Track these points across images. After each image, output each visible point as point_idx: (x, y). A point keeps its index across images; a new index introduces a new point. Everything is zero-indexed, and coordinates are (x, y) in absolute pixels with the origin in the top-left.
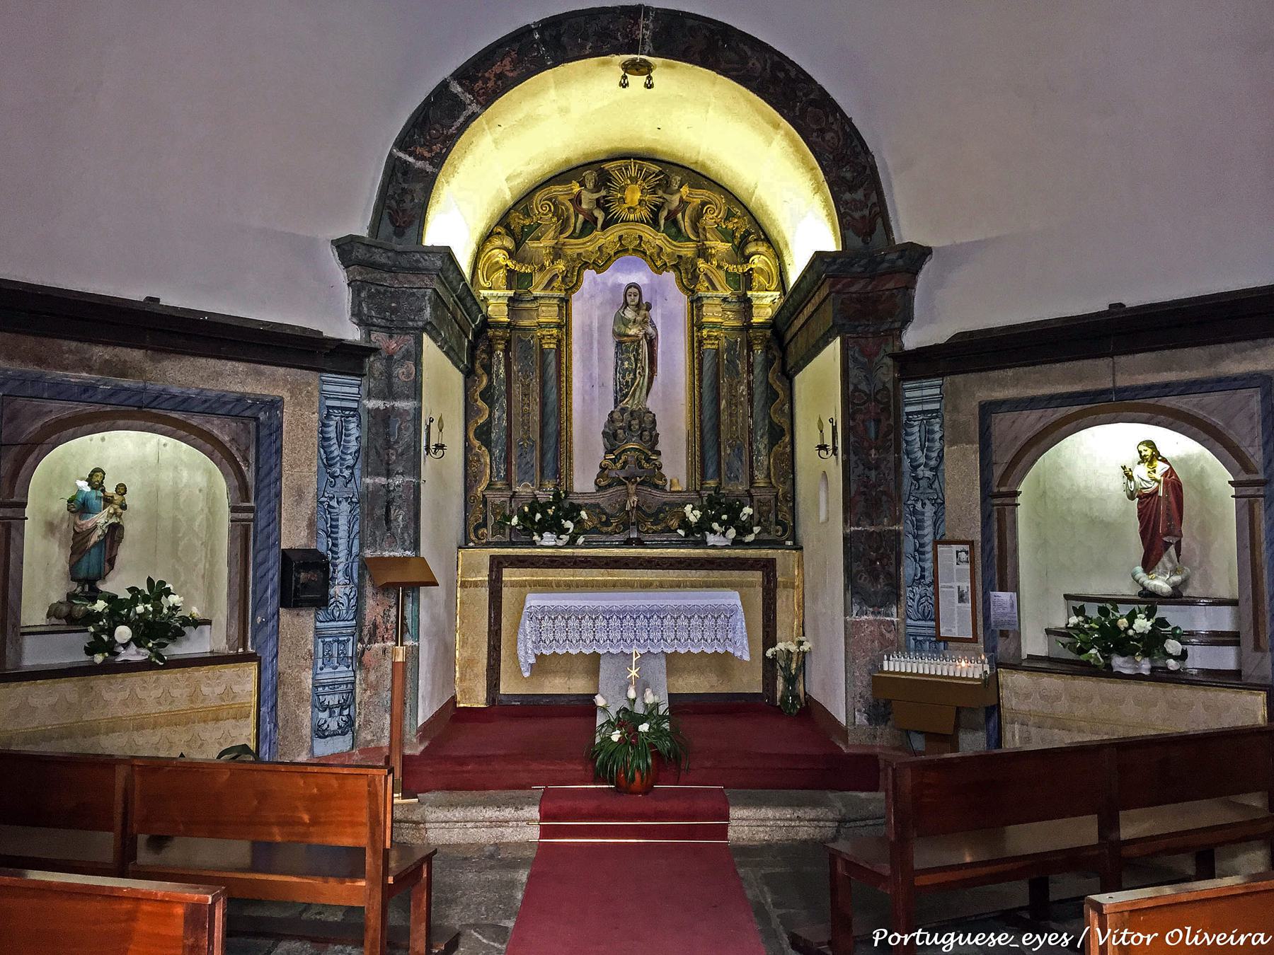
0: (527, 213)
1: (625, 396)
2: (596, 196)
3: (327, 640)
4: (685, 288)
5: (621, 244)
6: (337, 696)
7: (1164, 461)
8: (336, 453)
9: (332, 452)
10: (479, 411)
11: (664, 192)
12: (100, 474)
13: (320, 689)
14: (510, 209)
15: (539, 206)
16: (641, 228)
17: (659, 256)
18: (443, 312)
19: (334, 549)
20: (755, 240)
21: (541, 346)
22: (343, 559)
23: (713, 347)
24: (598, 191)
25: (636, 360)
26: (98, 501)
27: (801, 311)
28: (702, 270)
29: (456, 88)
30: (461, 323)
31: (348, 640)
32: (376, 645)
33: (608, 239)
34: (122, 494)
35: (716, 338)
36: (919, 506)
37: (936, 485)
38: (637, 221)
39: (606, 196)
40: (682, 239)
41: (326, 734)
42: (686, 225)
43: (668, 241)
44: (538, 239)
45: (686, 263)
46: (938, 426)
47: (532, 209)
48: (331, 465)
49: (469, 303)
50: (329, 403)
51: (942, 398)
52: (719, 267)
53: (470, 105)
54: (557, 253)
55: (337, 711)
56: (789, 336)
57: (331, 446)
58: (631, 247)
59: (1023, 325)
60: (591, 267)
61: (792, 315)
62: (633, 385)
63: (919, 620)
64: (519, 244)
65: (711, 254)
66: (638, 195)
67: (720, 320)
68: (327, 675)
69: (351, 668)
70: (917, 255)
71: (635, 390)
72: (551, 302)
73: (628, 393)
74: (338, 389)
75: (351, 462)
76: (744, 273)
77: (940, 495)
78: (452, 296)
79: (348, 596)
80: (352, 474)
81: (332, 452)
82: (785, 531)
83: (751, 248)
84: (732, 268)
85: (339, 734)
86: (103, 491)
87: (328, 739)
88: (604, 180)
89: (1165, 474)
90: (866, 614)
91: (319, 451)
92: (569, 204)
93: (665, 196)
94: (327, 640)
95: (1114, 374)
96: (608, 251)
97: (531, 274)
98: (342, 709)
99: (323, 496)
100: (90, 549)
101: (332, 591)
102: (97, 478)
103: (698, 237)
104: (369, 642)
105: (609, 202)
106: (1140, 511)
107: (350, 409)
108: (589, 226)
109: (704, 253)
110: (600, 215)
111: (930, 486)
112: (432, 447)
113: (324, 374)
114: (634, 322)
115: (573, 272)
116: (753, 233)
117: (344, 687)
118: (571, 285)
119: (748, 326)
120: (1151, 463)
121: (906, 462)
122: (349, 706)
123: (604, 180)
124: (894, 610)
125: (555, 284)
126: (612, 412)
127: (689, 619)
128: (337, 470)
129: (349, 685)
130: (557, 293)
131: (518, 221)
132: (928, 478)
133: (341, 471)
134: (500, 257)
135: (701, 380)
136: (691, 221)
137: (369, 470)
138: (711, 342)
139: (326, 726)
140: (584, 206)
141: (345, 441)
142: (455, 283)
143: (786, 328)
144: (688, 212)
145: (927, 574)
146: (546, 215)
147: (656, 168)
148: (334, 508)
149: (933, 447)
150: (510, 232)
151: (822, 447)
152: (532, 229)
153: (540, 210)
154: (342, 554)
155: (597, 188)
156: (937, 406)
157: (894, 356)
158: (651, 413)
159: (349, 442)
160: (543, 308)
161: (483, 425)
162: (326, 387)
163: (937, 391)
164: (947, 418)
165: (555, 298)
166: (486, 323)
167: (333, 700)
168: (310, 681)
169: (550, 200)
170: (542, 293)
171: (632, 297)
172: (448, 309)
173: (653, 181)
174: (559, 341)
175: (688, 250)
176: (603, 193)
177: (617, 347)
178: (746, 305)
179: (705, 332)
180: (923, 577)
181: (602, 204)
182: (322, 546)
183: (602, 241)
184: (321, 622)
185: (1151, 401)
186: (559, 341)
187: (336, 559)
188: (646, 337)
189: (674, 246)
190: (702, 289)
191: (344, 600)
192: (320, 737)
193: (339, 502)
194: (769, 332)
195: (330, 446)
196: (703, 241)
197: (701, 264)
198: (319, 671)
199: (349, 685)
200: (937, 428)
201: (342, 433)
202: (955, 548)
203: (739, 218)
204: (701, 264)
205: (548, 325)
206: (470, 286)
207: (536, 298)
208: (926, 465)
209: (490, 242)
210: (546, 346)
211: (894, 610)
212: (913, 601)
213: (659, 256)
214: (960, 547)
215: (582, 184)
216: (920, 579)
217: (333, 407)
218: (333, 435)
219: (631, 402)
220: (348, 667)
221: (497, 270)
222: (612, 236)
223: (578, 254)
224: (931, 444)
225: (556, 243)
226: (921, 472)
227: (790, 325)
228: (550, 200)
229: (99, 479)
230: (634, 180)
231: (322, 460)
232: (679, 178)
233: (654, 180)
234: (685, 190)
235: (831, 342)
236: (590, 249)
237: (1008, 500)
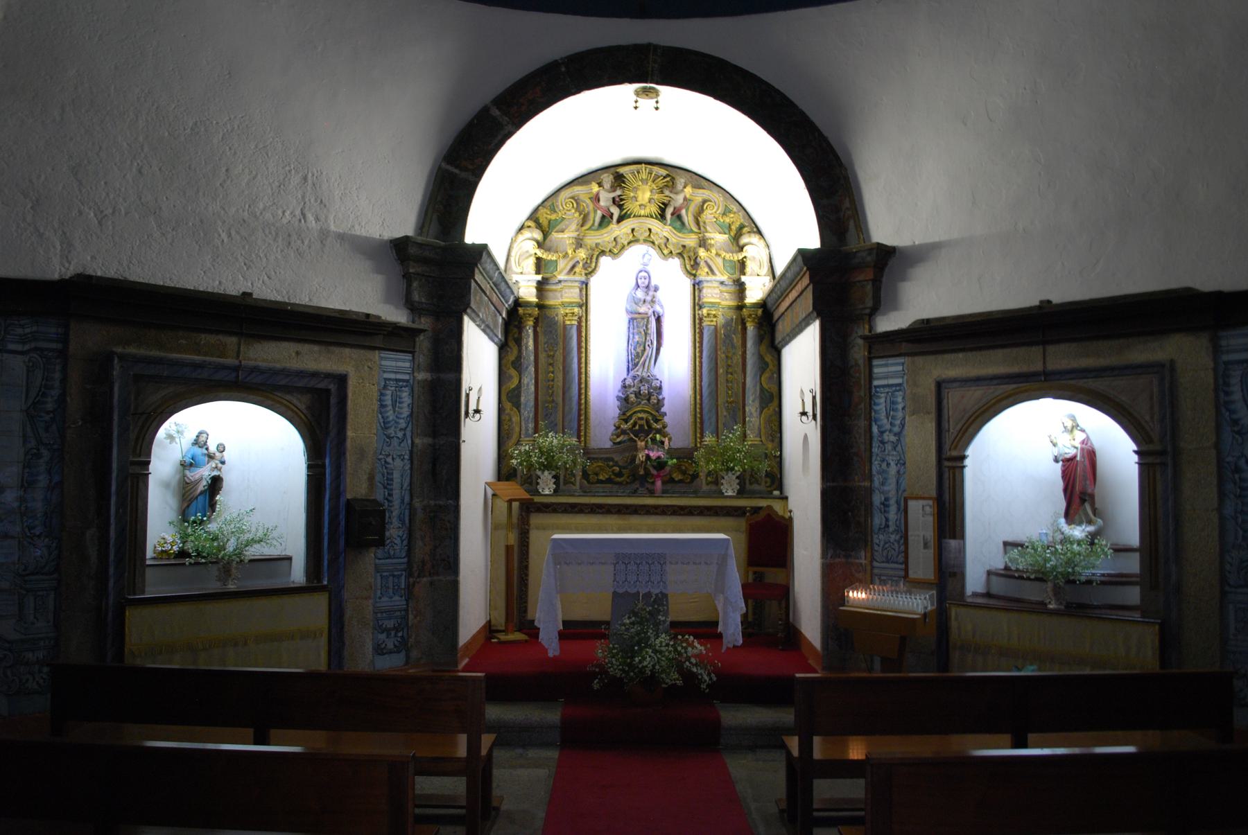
0: (553, 210)
1: (636, 365)
2: (613, 195)
3: (385, 574)
4: (689, 273)
5: (634, 235)
6: (392, 621)
7: (1083, 431)
8: (391, 418)
9: (388, 417)
10: (511, 377)
11: (671, 192)
12: (205, 435)
13: (379, 615)
14: (539, 206)
15: (564, 204)
16: (650, 222)
17: (666, 245)
18: (481, 297)
19: (390, 498)
20: (749, 232)
21: (564, 322)
22: (397, 507)
23: (712, 323)
24: (614, 191)
25: (646, 334)
26: (203, 457)
27: (788, 295)
28: (702, 258)
29: (496, 112)
30: (496, 305)
31: (402, 575)
32: (425, 579)
33: (621, 231)
34: (222, 452)
35: (715, 316)
36: (884, 465)
37: (899, 448)
38: (648, 216)
39: (621, 195)
40: (686, 231)
41: (385, 651)
42: (688, 218)
43: (674, 233)
44: (563, 231)
45: (689, 251)
46: (901, 398)
47: (558, 206)
48: (387, 428)
49: (503, 286)
50: (386, 376)
51: (904, 374)
52: (718, 255)
53: (506, 125)
54: (579, 243)
55: (393, 633)
56: (776, 317)
57: (387, 412)
58: (642, 238)
59: (971, 315)
60: (607, 254)
61: (780, 297)
62: (642, 355)
63: (883, 562)
64: (546, 235)
65: (710, 244)
66: (648, 195)
67: (718, 301)
68: (385, 602)
69: (403, 598)
70: (885, 254)
71: (645, 361)
72: (573, 285)
73: (638, 362)
74: (394, 364)
75: (403, 425)
76: (739, 261)
77: (902, 456)
78: (489, 283)
79: (401, 537)
80: (405, 435)
81: (388, 417)
82: (773, 482)
83: (744, 240)
84: (728, 256)
85: (394, 652)
86: (207, 449)
87: (386, 656)
88: (619, 180)
89: (1083, 442)
90: (839, 557)
91: (378, 417)
92: (588, 201)
93: (671, 195)
94: (385, 574)
95: (1044, 358)
96: (622, 241)
97: (556, 261)
98: (397, 631)
99: (381, 454)
100: (197, 497)
101: (387, 534)
102: (203, 438)
103: (700, 229)
104: (419, 577)
105: (622, 200)
106: (1063, 472)
107: (403, 381)
108: (606, 220)
109: (705, 243)
110: (616, 212)
111: (895, 448)
112: (471, 411)
113: (383, 352)
114: (644, 301)
115: (591, 259)
116: (747, 227)
117: (398, 613)
118: (590, 270)
119: (740, 307)
120: (1072, 431)
121: (875, 429)
122: (403, 629)
123: (619, 180)
124: (863, 553)
125: (577, 269)
126: (625, 379)
127: (638, 565)
128: (391, 431)
129: (403, 612)
130: (577, 278)
131: (544, 216)
132: (893, 442)
133: (396, 433)
134: (531, 247)
135: (701, 352)
136: (694, 216)
137: (419, 431)
138: (710, 319)
139: (384, 645)
140: (602, 203)
141: (399, 407)
142: (491, 272)
143: (774, 307)
144: (691, 209)
145: (890, 523)
146: (570, 210)
147: (663, 172)
148: (388, 463)
149: (896, 416)
150: (539, 226)
151: (804, 413)
152: (557, 222)
153: (565, 207)
154: (396, 503)
155: (613, 189)
156: (899, 381)
157: (865, 338)
158: (657, 379)
159: (401, 408)
160: (567, 290)
161: (514, 389)
162: (384, 363)
163: (900, 368)
164: (908, 392)
165: (576, 281)
166: (518, 303)
167: (390, 624)
168: (371, 608)
169: (573, 198)
170: (565, 278)
171: (643, 280)
172: (485, 294)
173: (660, 182)
174: (580, 318)
175: (691, 241)
176: (618, 192)
177: (629, 322)
178: (741, 288)
179: (705, 311)
180: (887, 526)
181: (619, 202)
182: (379, 495)
183: (617, 233)
184: (380, 559)
185: (1072, 382)
186: (580, 318)
187: (391, 506)
188: (654, 315)
189: (679, 237)
190: (703, 273)
191: (398, 541)
192: (379, 654)
193: (393, 459)
194: (760, 312)
195: (387, 412)
196: (704, 232)
197: (702, 253)
198: (378, 600)
199: (403, 612)
200: (900, 399)
201: (396, 401)
202: (921, 502)
203: (735, 213)
204: (702, 253)
205: (571, 304)
206: (503, 273)
207: (560, 282)
208: (890, 431)
209: (521, 233)
210: (568, 323)
211: (863, 553)
212: (879, 546)
213: (666, 245)
214: (925, 502)
215: (600, 185)
216: (884, 528)
217: (390, 379)
218: (389, 402)
219: (641, 370)
220: (401, 597)
221: (527, 258)
222: (625, 229)
223: (596, 244)
224: (895, 414)
225: (579, 235)
226: (886, 437)
227: (778, 305)
228: (573, 198)
229: (204, 439)
230: (644, 182)
231: (380, 424)
232: (683, 181)
233: (662, 181)
234: (688, 190)
235: (811, 323)
236: (607, 239)
237: (955, 464)
